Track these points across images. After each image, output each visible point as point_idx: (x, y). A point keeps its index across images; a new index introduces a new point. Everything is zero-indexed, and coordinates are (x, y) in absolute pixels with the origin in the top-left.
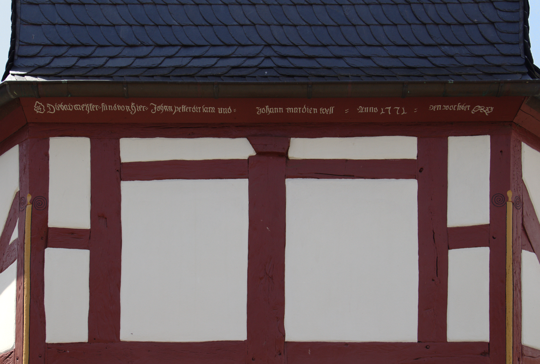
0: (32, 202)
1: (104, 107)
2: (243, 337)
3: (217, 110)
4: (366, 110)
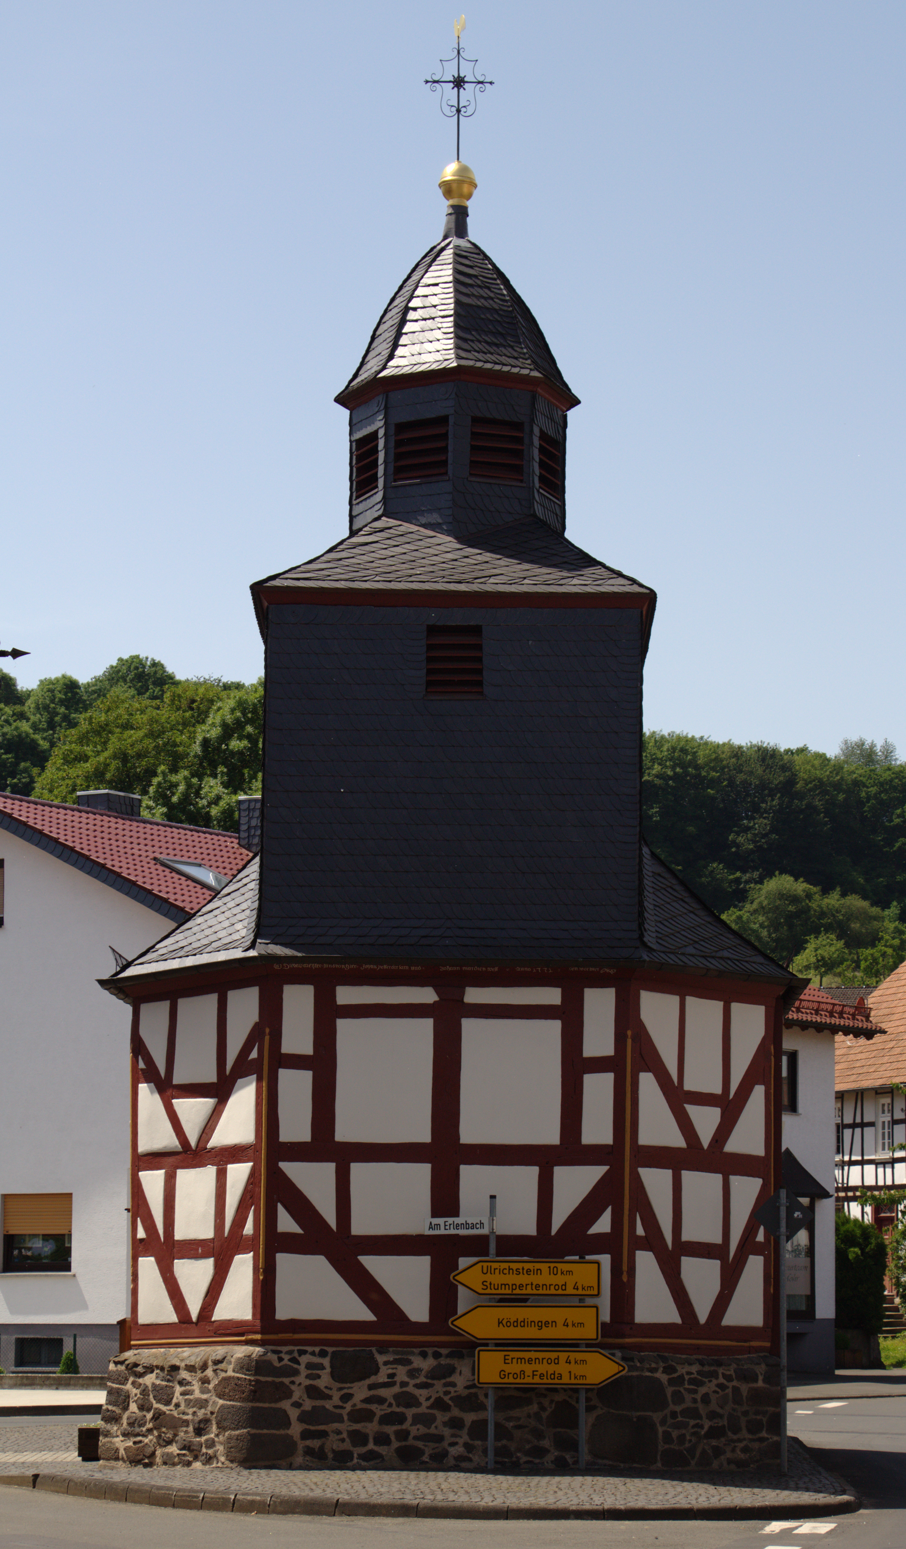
0: (270, 1034)
1: (326, 966)
2: (463, 1168)
3: (410, 968)
4: (522, 969)
